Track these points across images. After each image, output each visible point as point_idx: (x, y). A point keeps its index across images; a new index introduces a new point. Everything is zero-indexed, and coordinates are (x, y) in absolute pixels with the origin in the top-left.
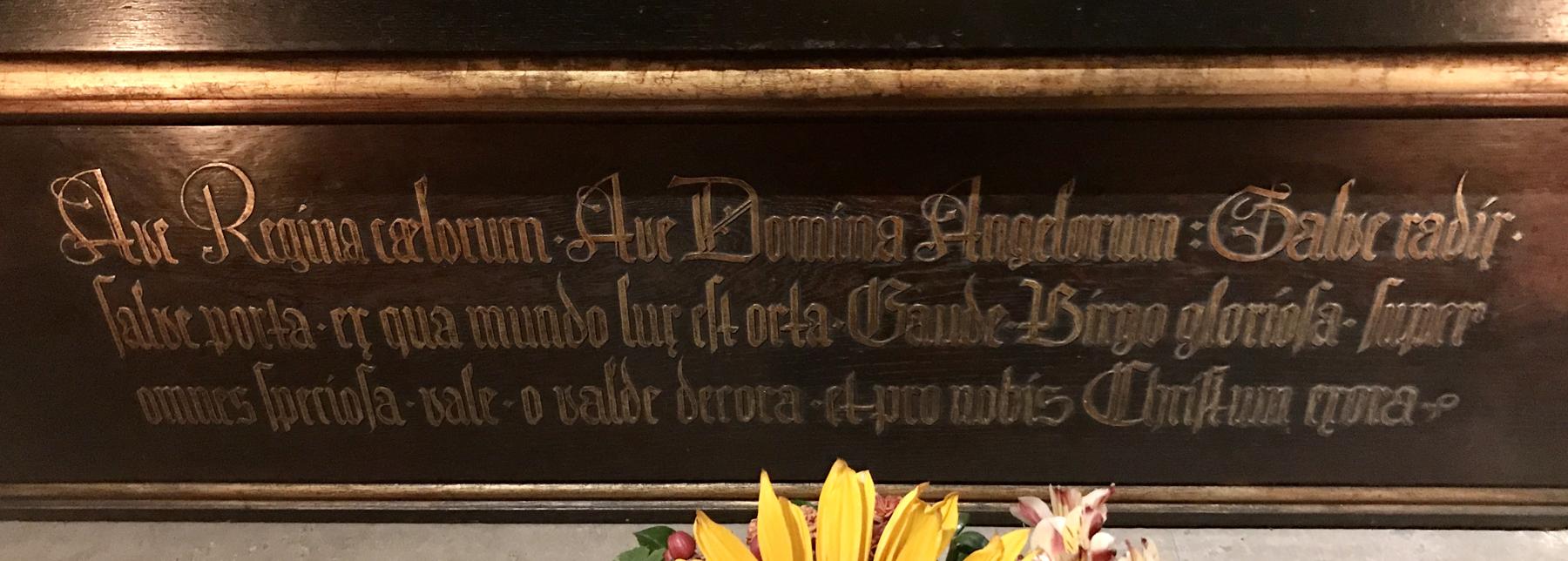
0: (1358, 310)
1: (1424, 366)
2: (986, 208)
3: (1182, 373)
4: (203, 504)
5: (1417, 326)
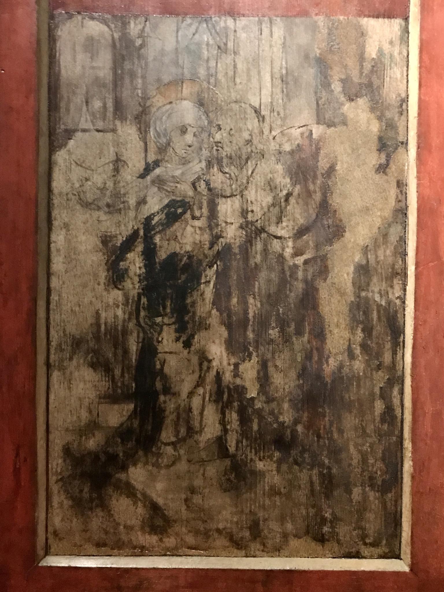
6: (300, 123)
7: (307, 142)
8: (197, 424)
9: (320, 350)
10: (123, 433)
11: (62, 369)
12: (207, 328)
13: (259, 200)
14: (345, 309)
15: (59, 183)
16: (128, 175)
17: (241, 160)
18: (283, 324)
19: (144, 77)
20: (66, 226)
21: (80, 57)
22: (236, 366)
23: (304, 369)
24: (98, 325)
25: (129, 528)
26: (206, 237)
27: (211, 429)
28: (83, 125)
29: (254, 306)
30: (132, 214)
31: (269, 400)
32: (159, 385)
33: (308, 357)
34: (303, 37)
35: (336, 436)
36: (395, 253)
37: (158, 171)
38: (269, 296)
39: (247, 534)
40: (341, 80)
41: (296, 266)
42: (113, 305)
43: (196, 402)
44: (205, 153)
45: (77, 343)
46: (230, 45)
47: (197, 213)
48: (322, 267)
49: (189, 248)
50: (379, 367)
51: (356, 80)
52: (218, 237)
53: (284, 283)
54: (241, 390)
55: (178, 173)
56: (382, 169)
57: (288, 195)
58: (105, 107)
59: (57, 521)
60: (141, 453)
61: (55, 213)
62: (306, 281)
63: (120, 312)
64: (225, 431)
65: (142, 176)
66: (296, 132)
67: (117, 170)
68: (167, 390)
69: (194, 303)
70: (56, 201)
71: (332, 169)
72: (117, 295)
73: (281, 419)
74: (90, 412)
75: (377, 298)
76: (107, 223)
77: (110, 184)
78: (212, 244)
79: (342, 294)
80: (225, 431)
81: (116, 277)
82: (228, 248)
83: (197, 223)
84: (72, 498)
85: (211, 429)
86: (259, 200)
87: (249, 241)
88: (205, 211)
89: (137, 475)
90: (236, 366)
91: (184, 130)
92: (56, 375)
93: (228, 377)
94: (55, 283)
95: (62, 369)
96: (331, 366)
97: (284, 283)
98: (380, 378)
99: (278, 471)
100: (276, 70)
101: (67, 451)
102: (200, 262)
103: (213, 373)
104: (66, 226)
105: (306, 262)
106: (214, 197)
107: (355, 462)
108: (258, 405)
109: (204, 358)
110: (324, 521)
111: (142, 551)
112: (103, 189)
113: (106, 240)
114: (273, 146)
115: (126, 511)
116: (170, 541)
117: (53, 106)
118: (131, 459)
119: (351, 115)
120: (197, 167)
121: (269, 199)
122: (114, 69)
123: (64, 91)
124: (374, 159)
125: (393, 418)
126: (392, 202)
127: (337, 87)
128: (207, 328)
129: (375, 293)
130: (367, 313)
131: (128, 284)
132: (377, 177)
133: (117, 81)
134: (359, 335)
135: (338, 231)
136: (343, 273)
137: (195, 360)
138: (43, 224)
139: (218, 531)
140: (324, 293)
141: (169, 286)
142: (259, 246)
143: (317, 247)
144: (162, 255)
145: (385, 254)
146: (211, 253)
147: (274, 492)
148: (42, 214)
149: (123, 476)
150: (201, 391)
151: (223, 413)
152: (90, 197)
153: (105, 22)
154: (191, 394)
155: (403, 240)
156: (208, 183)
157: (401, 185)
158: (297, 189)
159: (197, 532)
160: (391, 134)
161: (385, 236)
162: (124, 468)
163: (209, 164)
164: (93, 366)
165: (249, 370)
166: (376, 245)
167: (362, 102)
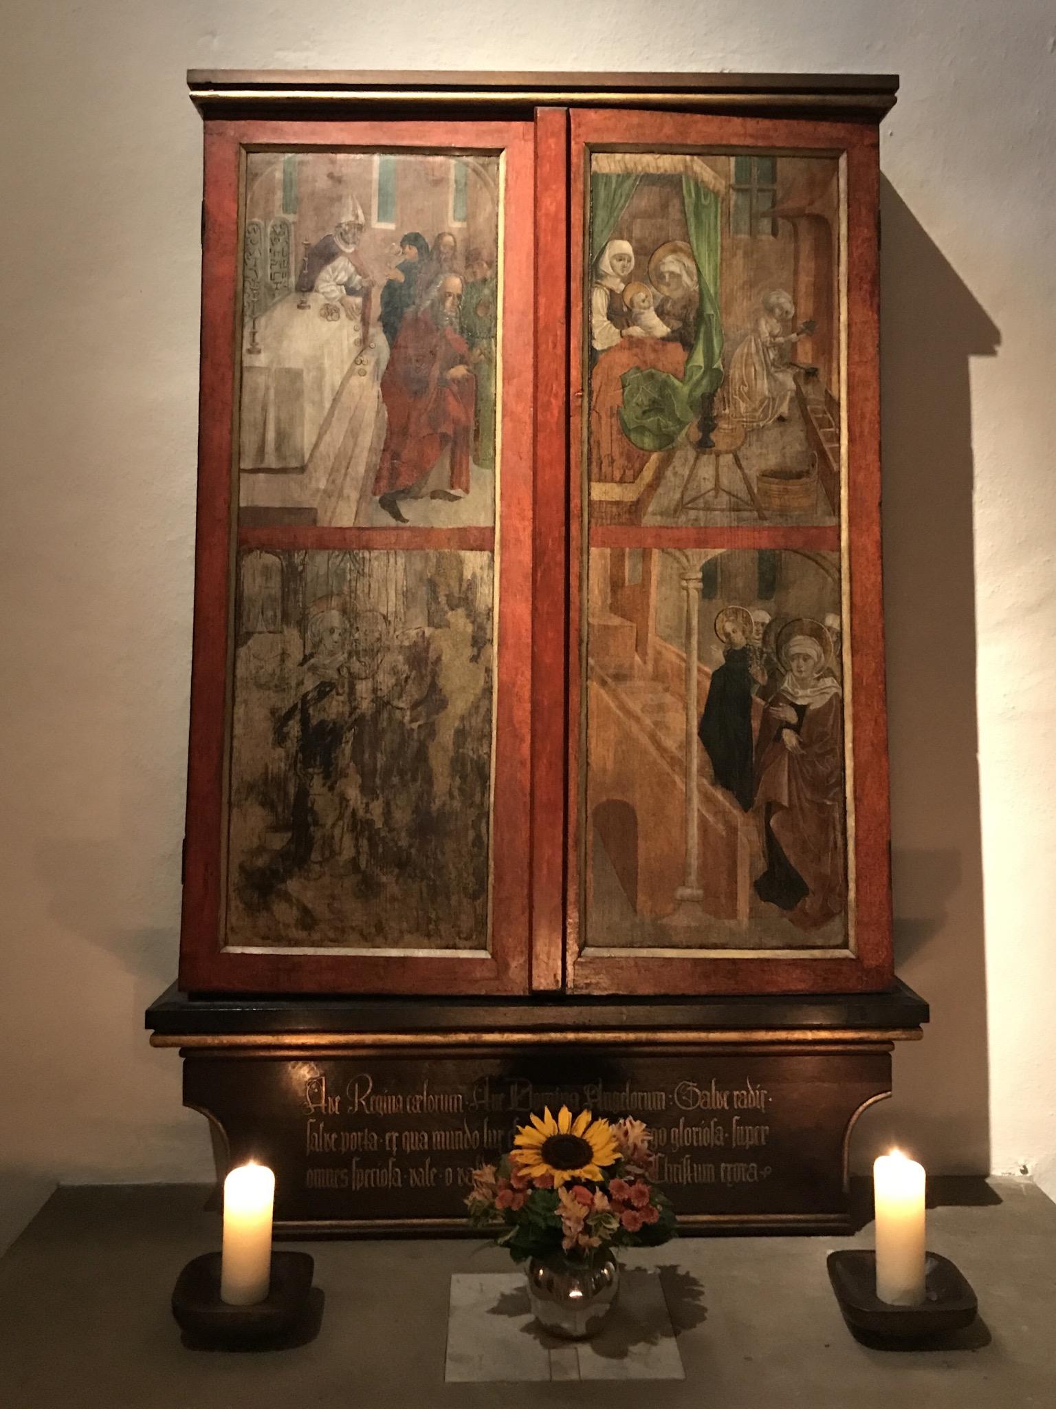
0: (728, 1128)
1: (753, 1154)
2: (605, 1089)
3: (675, 1159)
4: (660, 1049)
5: (750, 1136)
6: (416, 627)
7: (420, 640)
8: (337, 848)
9: (429, 793)
10: (283, 855)
11: (240, 806)
12: (346, 776)
13: (386, 681)
14: (447, 762)
15: (241, 671)
16: (291, 664)
17: (373, 653)
18: (402, 774)
19: (304, 594)
20: (245, 702)
21: (258, 580)
22: (367, 805)
23: (417, 807)
24: (266, 773)
25: (287, 926)
26: (347, 709)
27: (348, 852)
28: (259, 628)
29: (381, 760)
30: (293, 692)
31: (391, 830)
32: (310, 819)
33: (420, 798)
34: (418, 565)
35: (439, 857)
36: (483, 721)
37: (312, 661)
38: (392, 752)
39: (373, 930)
40: (447, 596)
41: (412, 730)
42: (277, 760)
43: (337, 832)
44: (347, 648)
45: (251, 787)
46: (366, 570)
47: (341, 691)
48: (431, 730)
49: (334, 717)
50: (471, 805)
51: (456, 595)
52: (355, 708)
53: (403, 743)
54: (370, 823)
55: (327, 662)
56: (475, 659)
57: (407, 678)
58: (275, 616)
59: (233, 920)
60: (296, 869)
61: (238, 692)
62: (419, 741)
63: (282, 765)
64: (358, 853)
65: (301, 664)
66: (413, 633)
67: (283, 661)
68: (316, 823)
69: (336, 758)
70: (238, 684)
71: (439, 659)
72: (280, 752)
73: (400, 844)
74: (259, 838)
75: (471, 753)
76: (275, 699)
77: (278, 672)
78: (351, 714)
79: (445, 750)
80: (358, 853)
81: (280, 738)
82: (363, 716)
83: (341, 698)
84: (246, 903)
85: (348, 852)
86: (386, 681)
87: (378, 712)
88: (346, 689)
89: (293, 886)
90: (367, 805)
91: (332, 631)
92: (235, 810)
93: (361, 813)
94: (236, 743)
95: (240, 806)
96: (436, 806)
97: (403, 743)
98: (472, 813)
99: (397, 882)
100: (399, 587)
101: (242, 867)
102: (342, 727)
103: (350, 810)
104: (245, 702)
105: (420, 726)
106: (353, 678)
107: (453, 876)
108: (383, 834)
109: (343, 799)
110: (429, 920)
111: (297, 944)
112: (273, 674)
113: (273, 712)
114: (397, 643)
115: (284, 912)
116: (316, 936)
117: (238, 616)
118: (289, 874)
119: (452, 620)
120: (341, 657)
121: (393, 681)
122: (283, 587)
123: (246, 604)
124: (469, 652)
125: (481, 842)
126: (482, 683)
127: (443, 599)
128: (346, 776)
129: (469, 750)
130: (463, 765)
131: (289, 744)
132: (471, 665)
133: (285, 597)
134: (458, 781)
135: (443, 704)
136: (446, 736)
137: (337, 800)
138: (229, 702)
139: (353, 928)
140: (432, 750)
141: (317, 744)
142: (385, 715)
143: (428, 716)
144: (314, 722)
145: (477, 721)
146: (350, 720)
147: (393, 899)
148: (229, 695)
149: (282, 886)
150: (341, 823)
151: (357, 839)
152: (263, 681)
153: (276, 555)
154: (334, 825)
155: (489, 710)
156: (349, 669)
157: (488, 671)
158: (414, 673)
159: (336, 929)
160: (481, 634)
161: (477, 707)
162: (284, 881)
163: (350, 655)
164: (263, 804)
165: (377, 808)
166: (470, 714)
167: (461, 611)
